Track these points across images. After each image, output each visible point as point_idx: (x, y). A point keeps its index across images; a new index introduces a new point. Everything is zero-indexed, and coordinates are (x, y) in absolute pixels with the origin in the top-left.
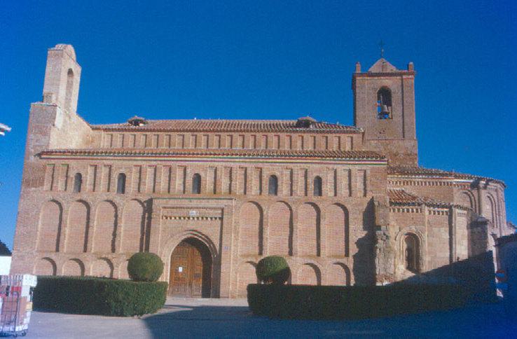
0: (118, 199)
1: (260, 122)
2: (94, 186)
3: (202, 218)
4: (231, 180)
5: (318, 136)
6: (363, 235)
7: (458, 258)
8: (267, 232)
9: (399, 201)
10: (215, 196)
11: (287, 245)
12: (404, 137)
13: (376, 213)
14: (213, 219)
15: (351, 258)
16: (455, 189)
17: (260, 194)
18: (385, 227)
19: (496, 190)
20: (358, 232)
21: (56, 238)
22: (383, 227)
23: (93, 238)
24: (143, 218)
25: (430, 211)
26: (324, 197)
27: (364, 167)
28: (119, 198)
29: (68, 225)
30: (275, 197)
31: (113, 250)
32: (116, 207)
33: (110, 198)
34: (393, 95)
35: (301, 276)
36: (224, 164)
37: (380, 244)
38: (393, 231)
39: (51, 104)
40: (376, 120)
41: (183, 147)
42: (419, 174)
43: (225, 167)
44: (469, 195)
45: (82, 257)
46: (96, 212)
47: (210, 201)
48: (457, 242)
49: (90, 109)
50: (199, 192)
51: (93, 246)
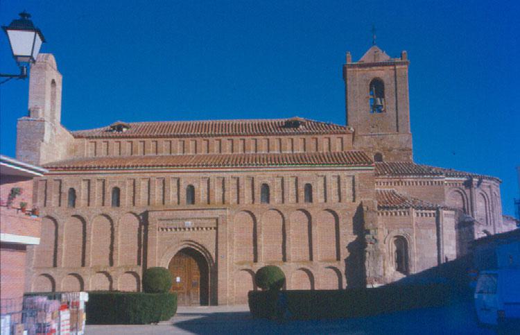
0: (113, 213)
1: (248, 121)
2: (89, 201)
3: (198, 228)
4: (224, 191)
5: (308, 138)
6: (354, 239)
7: (447, 259)
8: (261, 240)
9: (390, 204)
10: (208, 207)
11: (281, 252)
12: (398, 131)
13: (365, 218)
14: (209, 229)
15: (342, 262)
16: (446, 189)
17: (253, 203)
18: (373, 231)
19: (490, 187)
20: (348, 237)
21: (53, 254)
22: (372, 231)
23: (91, 253)
24: (140, 230)
25: (418, 214)
26: (314, 203)
27: (352, 173)
28: (114, 212)
29: (64, 241)
30: (268, 205)
31: (111, 263)
32: (111, 221)
33: (105, 211)
34: (386, 87)
35: (295, 282)
36: (217, 174)
37: (370, 247)
38: (382, 234)
39: (38, 119)
40: (369, 114)
41: (171, 153)
42: (410, 174)
43: (218, 178)
44: (460, 193)
45: (81, 271)
46: (92, 226)
47: (205, 211)
48: (445, 242)
49: (70, 120)
50: (193, 202)
51: (91, 260)
